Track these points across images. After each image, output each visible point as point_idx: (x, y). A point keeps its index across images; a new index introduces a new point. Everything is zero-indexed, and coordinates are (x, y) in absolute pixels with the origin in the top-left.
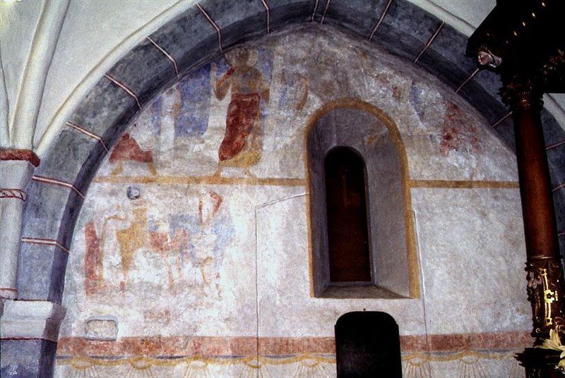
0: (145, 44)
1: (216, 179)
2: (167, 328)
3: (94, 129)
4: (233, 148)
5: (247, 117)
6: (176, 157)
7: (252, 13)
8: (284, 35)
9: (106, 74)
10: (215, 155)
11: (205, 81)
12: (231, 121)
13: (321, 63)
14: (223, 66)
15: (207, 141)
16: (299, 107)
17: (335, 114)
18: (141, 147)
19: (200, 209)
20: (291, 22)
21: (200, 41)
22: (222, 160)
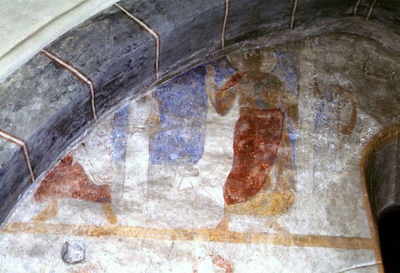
0: (112, 12)
1: (220, 233)
2: (248, 202)
3: (14, 128)
4: (248, 186)
6: (150, 196)
10: (217, 195)
12: (241, 144)
15: (204, 174)
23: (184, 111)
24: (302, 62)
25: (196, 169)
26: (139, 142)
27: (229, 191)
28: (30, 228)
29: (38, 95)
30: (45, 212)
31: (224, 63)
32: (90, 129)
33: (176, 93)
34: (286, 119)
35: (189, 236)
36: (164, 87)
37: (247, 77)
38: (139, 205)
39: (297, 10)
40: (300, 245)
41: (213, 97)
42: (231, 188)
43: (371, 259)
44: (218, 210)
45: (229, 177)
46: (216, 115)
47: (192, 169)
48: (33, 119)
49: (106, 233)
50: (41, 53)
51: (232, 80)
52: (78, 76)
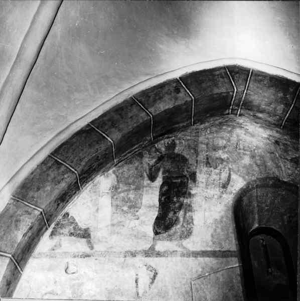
0: (87, 129)
1: (150, 252)
2: (167, 233)
3: (37, 201)
4: (167, 223)
5: (178, 196)
6: (112, 233)
7: (179, 103)
8: (206, 128)
9: (51, 154)
10: (149, 230)
11: (138, 166)
12: (163, 199)
13: (240, 149)
14: (154, 154)
15: (142, 218)
16: (225, 186)
17: (257, 193)
18: (79, 224)
19: (136, 282)
20: (212, 116)
21: (135, 125)
22: (156, 235)
23: (131, 181)
24: (200, 145)
25: (138, 215)
26: (106, 201)
27: (156, 227)
28: (47, 255)
29: (49, 181)
30: (55, 246)
31: (154, 149)
32: (79, 195)
33: (126, 170)
34: (189, 182)
35: (133, 255)
36: (119, 167)
37: (167, 157)
38: (106, 238)
39: (194, 116)
40: (195, 257)
41: (148, 171)
42: (157, 226)
43: (236, 263)
44: (150, 239)
45: (156, 219)
46: (149, 182)
47: (135, 215)
48: (46, 195)
49: (88, 256)
50: (49, 156)
51: (158, 160)
52: (69, 169)
